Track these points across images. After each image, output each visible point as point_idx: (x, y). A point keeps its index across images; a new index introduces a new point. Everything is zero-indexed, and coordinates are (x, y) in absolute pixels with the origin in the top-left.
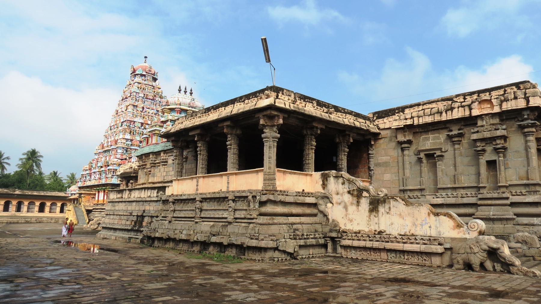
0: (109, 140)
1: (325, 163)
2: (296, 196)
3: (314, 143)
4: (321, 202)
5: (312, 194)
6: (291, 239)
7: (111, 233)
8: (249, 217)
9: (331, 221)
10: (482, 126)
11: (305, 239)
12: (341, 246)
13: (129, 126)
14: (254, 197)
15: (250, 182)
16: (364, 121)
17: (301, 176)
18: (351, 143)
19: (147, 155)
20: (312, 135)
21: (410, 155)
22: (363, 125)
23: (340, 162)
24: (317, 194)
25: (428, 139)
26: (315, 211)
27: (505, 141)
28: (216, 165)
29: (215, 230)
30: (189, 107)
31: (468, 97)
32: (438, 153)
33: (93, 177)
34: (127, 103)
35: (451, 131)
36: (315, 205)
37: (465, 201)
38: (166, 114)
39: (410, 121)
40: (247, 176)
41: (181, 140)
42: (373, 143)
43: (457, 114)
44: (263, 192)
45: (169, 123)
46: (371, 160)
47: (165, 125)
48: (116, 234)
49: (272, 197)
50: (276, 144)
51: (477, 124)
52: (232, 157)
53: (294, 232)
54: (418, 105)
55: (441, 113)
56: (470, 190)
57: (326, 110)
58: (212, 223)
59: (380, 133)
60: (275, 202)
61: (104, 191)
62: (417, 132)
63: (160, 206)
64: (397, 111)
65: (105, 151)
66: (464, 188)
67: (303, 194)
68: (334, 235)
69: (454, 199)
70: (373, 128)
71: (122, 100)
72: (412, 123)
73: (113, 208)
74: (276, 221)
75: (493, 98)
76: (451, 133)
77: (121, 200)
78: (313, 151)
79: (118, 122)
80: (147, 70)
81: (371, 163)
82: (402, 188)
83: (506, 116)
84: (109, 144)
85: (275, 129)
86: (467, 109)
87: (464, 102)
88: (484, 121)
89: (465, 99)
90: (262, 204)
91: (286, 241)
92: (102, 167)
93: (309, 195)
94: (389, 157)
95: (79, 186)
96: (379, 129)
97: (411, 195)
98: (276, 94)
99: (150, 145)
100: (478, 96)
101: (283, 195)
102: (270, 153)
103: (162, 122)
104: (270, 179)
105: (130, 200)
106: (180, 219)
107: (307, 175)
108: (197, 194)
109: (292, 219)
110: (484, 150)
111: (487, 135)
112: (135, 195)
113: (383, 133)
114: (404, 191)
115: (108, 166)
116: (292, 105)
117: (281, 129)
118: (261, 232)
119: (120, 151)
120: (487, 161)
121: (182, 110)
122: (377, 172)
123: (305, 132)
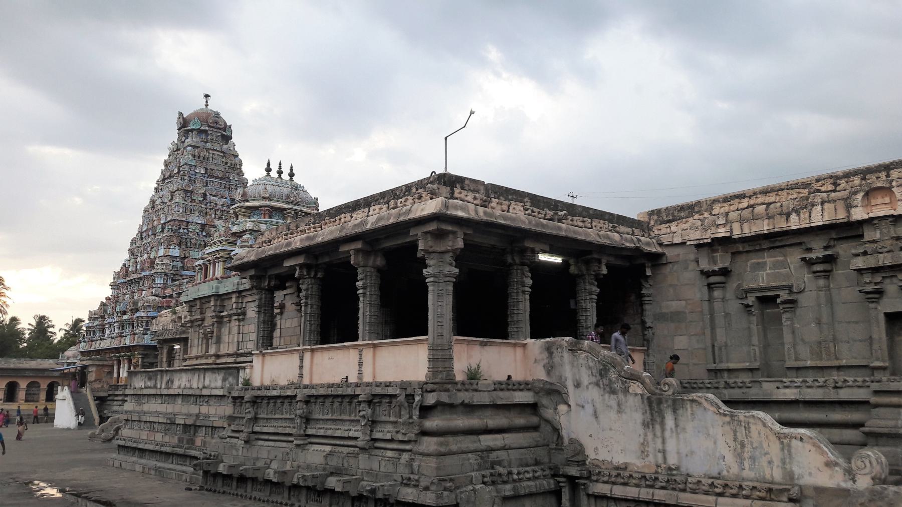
0: (138, 259)
1: (554, 318)
2: (495, 390)
3: (529, 282)
4: (545, 401)
5: (527, 384)
6: (484, 483)
7: (134, 459)
8: (400, 437)
9: (566, 441)
10: (874, 242)
11: (514, 481)
12: (588, 495)
13: (176, 232)
14: (410, 397)
15: (403, 363)
16: (629, 230)
18: (604, 275)
19: (205, 300)
20: (523, 264)
21: (728, 301)
22: (626, 240)
23: (582, 316)
24: (536, 384)
26: (534, 420)
29: (334, 462)
30: (287, 203)
31: (843, 183)
32: (784, 296)
33: (107, 332)
35: (809, 250)
36: (533, 407)
37: (844, 394)
38: (241, 219)
39: (723, 230)
40: (397, 349)
41: (268, 275)
42: (649, 272)
43: (818, 218)
44: (424, 388)
46: (647, 307)
47: (239, 241)
48: (143, 461)
49: (445, 398)
50: (450, 288)
51: (862, 236)
52: (366, 309)
53: (493, 468)
54: (741, 196)
55: (788, 215)
56: (853, 371)
57: (550, 213)
58: (328, 449)
59: (663, 255)
60: (451, 407)
61: (130, 361)
62: (740, 253)
63: (227, 409)
64: (696, 209)
65: (131, 282)
66: (839, 368)
67: (509, 384)
68: (573, 471)
69: (820, 391)
70: (648, 244)
71: (164, 180)
72: (728, 234)
73: (138, 409)
74: (454, 448)
75: (894, 184)
76: (809, 256)
77: (153, 391)
78: (527, 297)
79: (155, 224)
80: (210, 121)
81: (647, 313)
82: (713, 366)
84: (138, 267)
85: (448, 258)
86: (840, 205)
87: (835, 191)
88: (878, 232)
89: (835, 184)
90: (426, 411)
91: (474, 490)
92: (124, 313)
93: (524, 386)
94: (684, 303)
95: (81, 350)
96: (661, 245)
97: (731, 381)
98: (449, 188)
99: (212, 279)
100: (864, 179)
101: (466, 390)
102: (440, 305)
103: (234, 234)
104: (440, 360)
105: (171, 392)
106: (266, 437)
107: (515, 345)
108: (298, 386)
109: (487, 440)
110: (880, 293)
111: (886, 260)
112: (181, 382)
113: (670, 253)
114: (716, 372)
115: (137, 310)
116: (481, 210)
117: (459, 258)
118: (425, 472)
119: (159, 281)
120: (885, 314)
121: (273, 211)
122: (661, 331)
123: (509, 260)
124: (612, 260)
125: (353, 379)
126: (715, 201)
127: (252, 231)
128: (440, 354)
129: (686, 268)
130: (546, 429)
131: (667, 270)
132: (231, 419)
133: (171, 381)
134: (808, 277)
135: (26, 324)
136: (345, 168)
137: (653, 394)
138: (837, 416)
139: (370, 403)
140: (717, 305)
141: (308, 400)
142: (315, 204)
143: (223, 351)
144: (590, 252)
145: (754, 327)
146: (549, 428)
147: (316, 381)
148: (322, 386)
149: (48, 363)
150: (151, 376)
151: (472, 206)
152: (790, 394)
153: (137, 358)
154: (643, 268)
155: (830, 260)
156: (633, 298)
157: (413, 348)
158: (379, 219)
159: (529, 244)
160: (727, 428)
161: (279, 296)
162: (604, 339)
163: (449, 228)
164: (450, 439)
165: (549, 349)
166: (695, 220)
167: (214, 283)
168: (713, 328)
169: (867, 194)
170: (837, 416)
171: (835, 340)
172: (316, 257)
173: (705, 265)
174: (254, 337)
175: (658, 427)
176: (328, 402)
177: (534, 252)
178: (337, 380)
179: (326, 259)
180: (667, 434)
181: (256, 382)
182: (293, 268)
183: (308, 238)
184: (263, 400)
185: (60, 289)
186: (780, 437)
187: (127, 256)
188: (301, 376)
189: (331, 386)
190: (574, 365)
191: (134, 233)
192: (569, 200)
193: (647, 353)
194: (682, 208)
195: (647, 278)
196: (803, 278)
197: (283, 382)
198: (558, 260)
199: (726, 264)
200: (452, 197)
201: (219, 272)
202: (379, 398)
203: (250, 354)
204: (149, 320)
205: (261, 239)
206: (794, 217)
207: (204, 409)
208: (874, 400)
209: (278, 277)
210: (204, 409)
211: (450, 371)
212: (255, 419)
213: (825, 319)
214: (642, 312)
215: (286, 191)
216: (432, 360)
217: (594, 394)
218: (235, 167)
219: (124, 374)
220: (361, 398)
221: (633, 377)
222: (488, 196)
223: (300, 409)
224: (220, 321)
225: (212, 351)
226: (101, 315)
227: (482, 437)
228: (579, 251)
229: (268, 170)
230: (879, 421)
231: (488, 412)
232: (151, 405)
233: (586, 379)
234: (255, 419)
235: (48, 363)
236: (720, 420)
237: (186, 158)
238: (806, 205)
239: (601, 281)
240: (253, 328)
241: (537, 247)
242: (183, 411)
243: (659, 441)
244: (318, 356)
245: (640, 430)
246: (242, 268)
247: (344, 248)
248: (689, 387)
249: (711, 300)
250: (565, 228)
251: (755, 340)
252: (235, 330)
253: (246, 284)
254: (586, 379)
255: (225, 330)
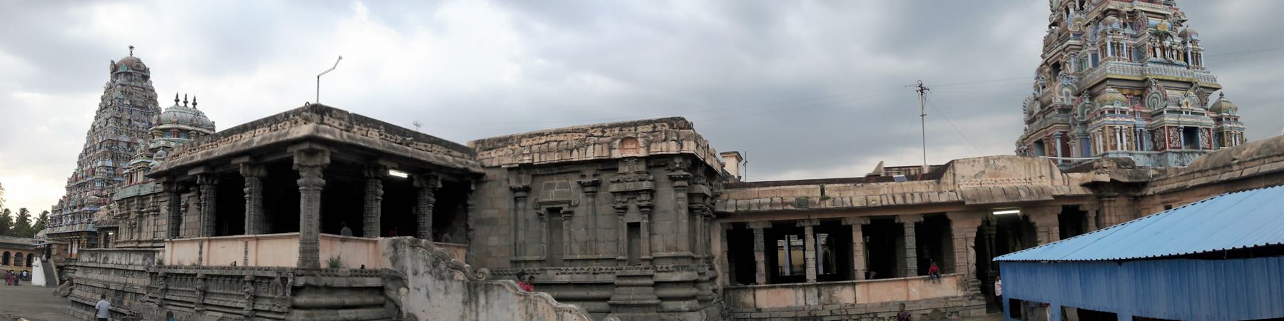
1: (399, 221)
4: (390, 285)
8: (276, 309)
9: (405, 315)
13: (110, 148)
14: (284, 280)
15: (280, 253)
17: (359, 245)
20: (377, 178)
21: (528, 211)
23: (421, 220)
25: (551, 186)
26: (381, 299)
27: (652, 196)
28: (226, 222)
31: (608, 131)
32: (566, 208)
34: (108, 115)
35: (584, 176)
36: (381, 290)
37: (599, 279)
40: (270, 242)
41: (176, 181)
42: (473, 188)
43: (591, 154)
44: (295, 273)
45: (160, 152)
49: (311, 281)
50: (318, 195)
52: (251, 210)
54: (541, 134)
55: (571, 151)
57: (400, 139)
58: (220, 315)
60: (316, 288)
63: (146, 281)
65: (79, 185)
66: (597, 260)
67: (363, 272)
76: (583, 181)
82: (514, 258)
83: (655, 162)
85: (318, 171)
86: (605, 146)
89: (603, 132)
90: (296, 290)
93: (374, 273)
96: (483, 167)
102: (310, 209)
104: (309, 252)
107: (368, 242)
108: (198, 267)
110: (625, 209)
111: (630, 187)
112: (114, 260)
113: (489, 173)
114: (515, 263)
116: (345, 134)
117: (327, 172)
119: (98, 185)
121: (180, 132)
122: (480, 232)
124: (446, 177)
125: (240, 264)
126: (523, 136)
127: (165, 148)
128: (309, 247)
129: (500, 185)
130: (390, 305)
131: (486, 186)
132: (149, 288)
133: (106, 258)
134: (581, 195)
135: (14, 216)
136: (233, 99)
137: (470, 279)
138: (594, 293)
139: (253, 282)
140: (520, 213)
141: (206, 278)
142: (212, 126)
143: (143, 238)
144: (430, 171)
145: (544, 230)
146: (392, 305)
147: (212, 264)
148: (217, 268)
149: (27, 241)
150: (93, 254)
151: (337, 131)
152: (565, 278)
153: (84, 241)
154: (469, 184)
155: (596, 184)
156: (460, 207)
157: (287, 242)
158: (263, 139)
159: (382, 162)
160: (522, 305)
161: (184, 197)
162: (437, 237)
163: (319, 147)
164: (315, 312)
165: (395, 245)
166: (508, 149)
167: (137, 187)
168: (516, 231)
169: (622, 141)
170: (594, 293)
171: (596, 241)
172: (213, 169)
173: (513, 184)
174: (165, 228)
175: (473, 305)
176: (221, 280)
177: (386, 169)
178: (228, 264)
179: (221, 170)
180: (480, 309)
181: (167, 263)
182: (195, 176)
183: (207, 153)
184: (172, 276)
185: (36, 192)
186: (556, 310)
187: (76, 166)
188: (200, 259)
189: (223, 268)
190: (415, 258)
191: (81, 150)
192: (414, 129)
193: (468, 249)
194: (500, 140)
195: (471, 192)
196: (578, 196)
197: (187, 264)
198: (404, 175)
199: (528, 183)
200: (322, 123)
201: (140, 179)
202: (260, 279)
203: (163, 241)
204: (92, 213)
205: (171, 154)
206: (575, 152)
207: (130, 280)
208: (617, 282)
209: (184, 183)
210: (130, 280)
211: (316, 260)
212: (166, 290)
213: (590, 226)
214: (466, 218)
215: (190, 116)
216: (303, 251)
217: (428, 280)
218: (151, 98)
219: (75, 251)
220: (246, 279)
221: (458, 268)
222: (351, 122)
223: (199, 285)
224: (141, 215)
225: (135, 238)
226: (59, 209)
227: (340, 312)
228: (418, 168)
229: (177, 101)
230: (620, 296)
231: (346, 293)
232: (94, 272)
233: (422, 269)
234: (166, 290)
235: (27, 241)
236: (517, 299)
237: (117, 93)
238: (583, 145)
239: (437, 193)
240: (165, 221)
241: (389, 164)
242: (115, 280)
243: (474, 314)
244: (213, 244)
245: (461, 306)
246: (157, 176)
247: (234, 162)
248: (497, 274)
249: (516, 209)
250: (410, 151)
251: (544, 239)
252: (152, 223)
253: (160, 188)
254: (422, 269)
255: (145, 223)
